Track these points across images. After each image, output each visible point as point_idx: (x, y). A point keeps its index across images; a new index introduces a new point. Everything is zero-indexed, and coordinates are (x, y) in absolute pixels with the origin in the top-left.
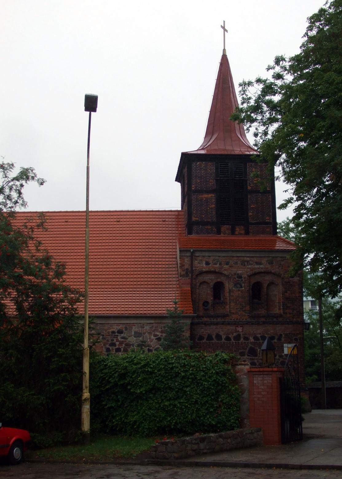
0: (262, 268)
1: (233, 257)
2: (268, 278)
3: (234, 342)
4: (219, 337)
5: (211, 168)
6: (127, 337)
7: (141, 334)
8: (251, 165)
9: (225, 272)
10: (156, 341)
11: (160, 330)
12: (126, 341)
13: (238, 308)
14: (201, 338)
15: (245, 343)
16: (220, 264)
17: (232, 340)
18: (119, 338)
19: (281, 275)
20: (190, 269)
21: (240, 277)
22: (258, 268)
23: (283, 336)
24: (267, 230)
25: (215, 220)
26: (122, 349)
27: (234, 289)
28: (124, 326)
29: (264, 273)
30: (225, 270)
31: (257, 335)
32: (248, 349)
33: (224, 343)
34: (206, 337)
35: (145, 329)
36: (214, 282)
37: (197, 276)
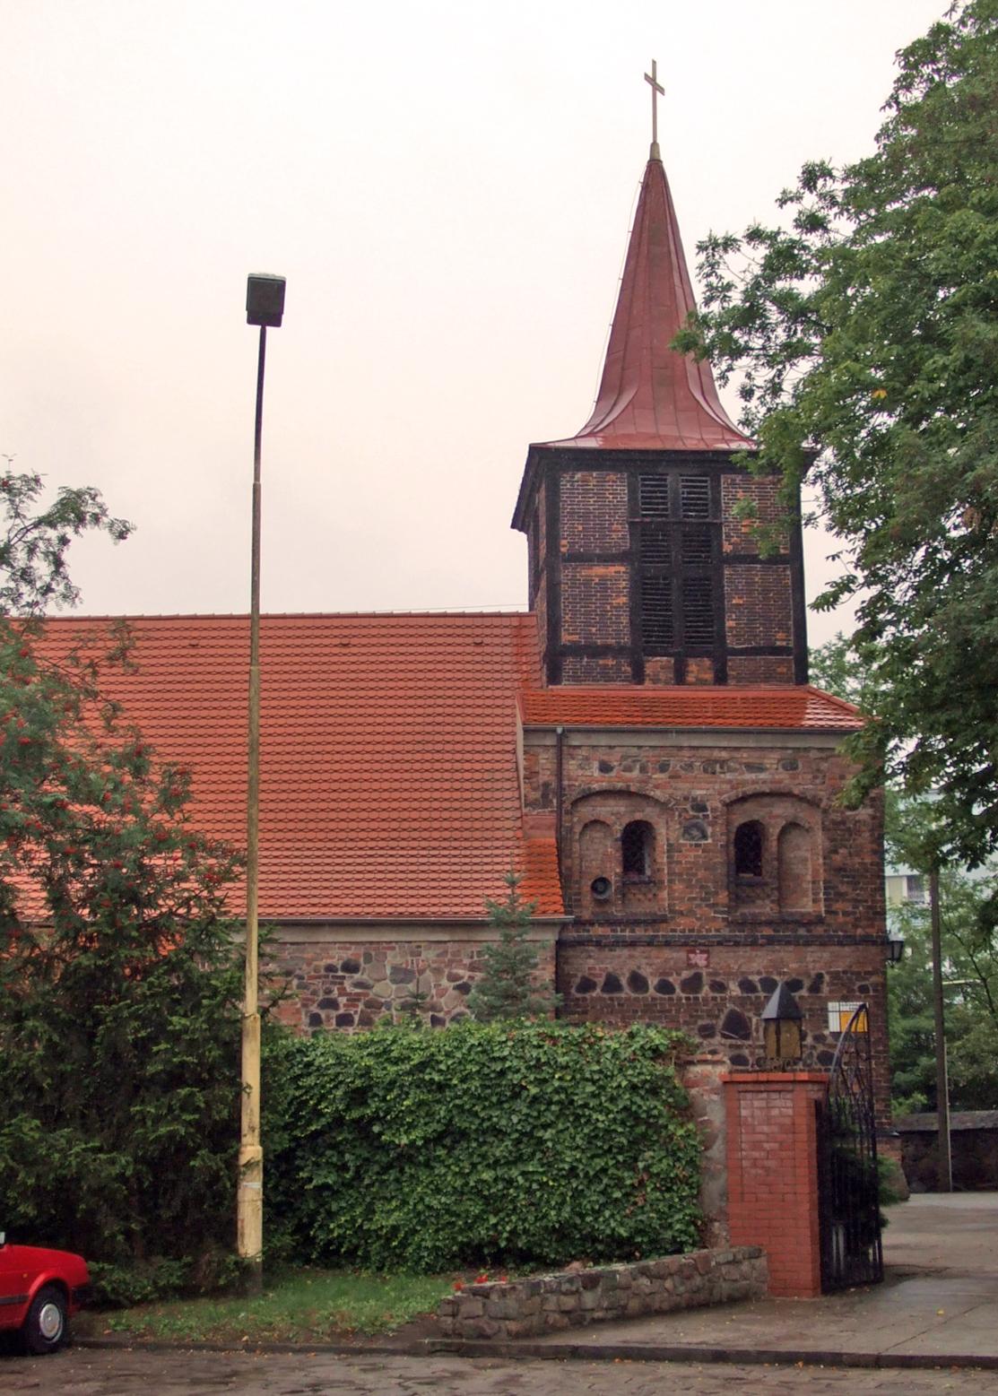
0: (764, 782)
1: (681, 748)
2: (781, 812)
3: (683, 995)
4: (638, 982)
5: (617, 489)
6: (371, 982)
7: (412, 972)
8: (733, 480)
9: (657, 794)
10: (456, 993)
11: (467, 961)
12: (367, 995)
13: (694, 899)
14: (587, 985)
15: (714, 999)
16: (643, 770)
17: (678, 990)
18: (347, 984)
19: (821, 800)
20: (554, 785)
21: (700, 807)
22: (754, 782)
23: (827, 978)
24: (779, 670)
25: (626, 640)
26: (356, 1018)
27: (681, 841)
28: (362, 950)
29: (771, 794)
30: (657, 787)
31: (750, 978)
32: (723, 1017)
34: (601, 981)
35: (423, 957)
36: (626, 821)
37: (575, 803)
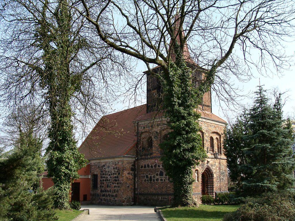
14: (142, 167)
33: (150, 169)
